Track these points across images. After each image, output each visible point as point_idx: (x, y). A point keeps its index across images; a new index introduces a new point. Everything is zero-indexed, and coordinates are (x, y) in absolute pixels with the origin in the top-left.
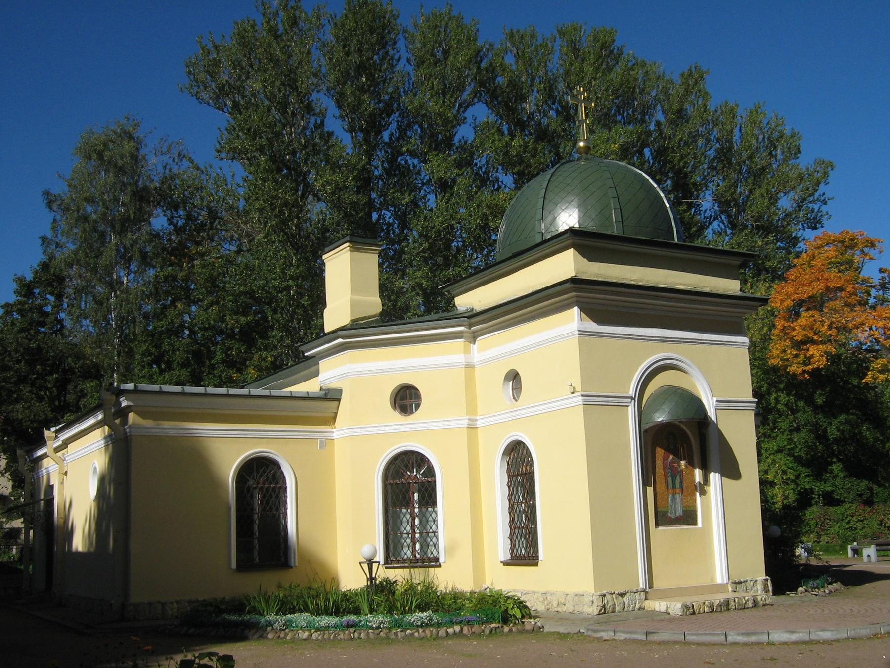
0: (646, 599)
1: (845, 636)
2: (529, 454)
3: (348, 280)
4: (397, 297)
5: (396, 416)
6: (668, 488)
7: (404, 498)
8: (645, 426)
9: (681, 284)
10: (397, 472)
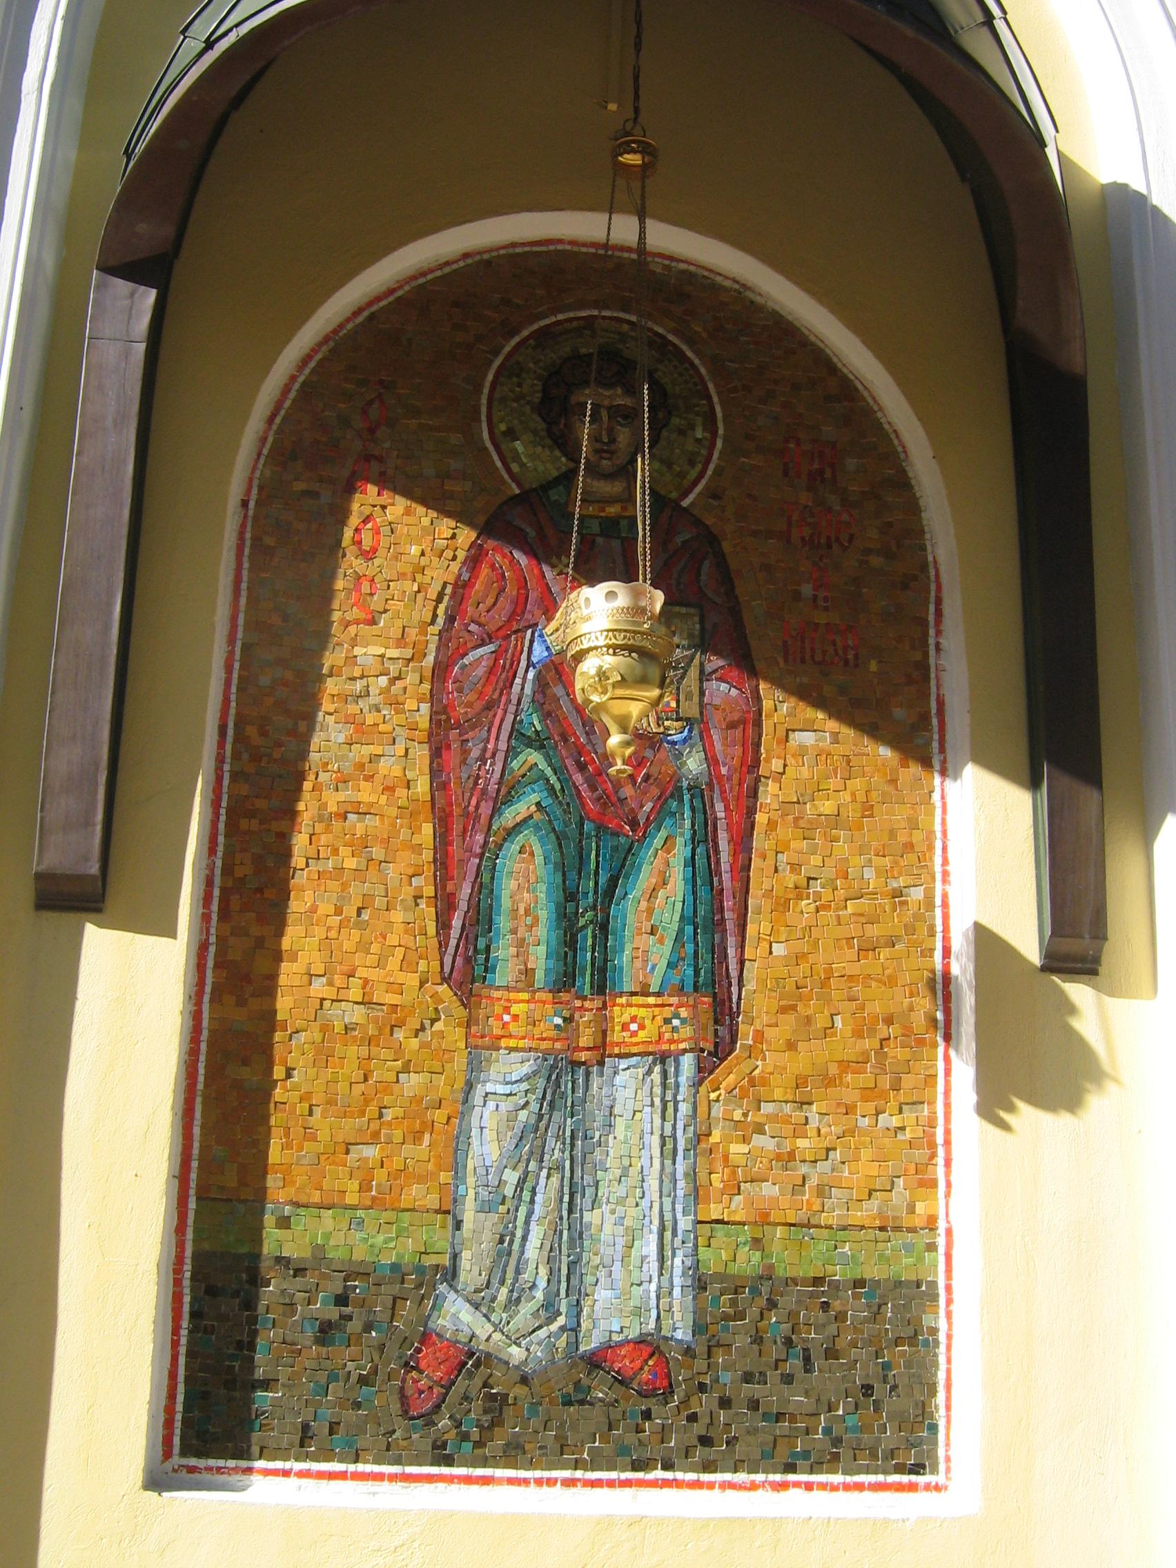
6: (468, 972)
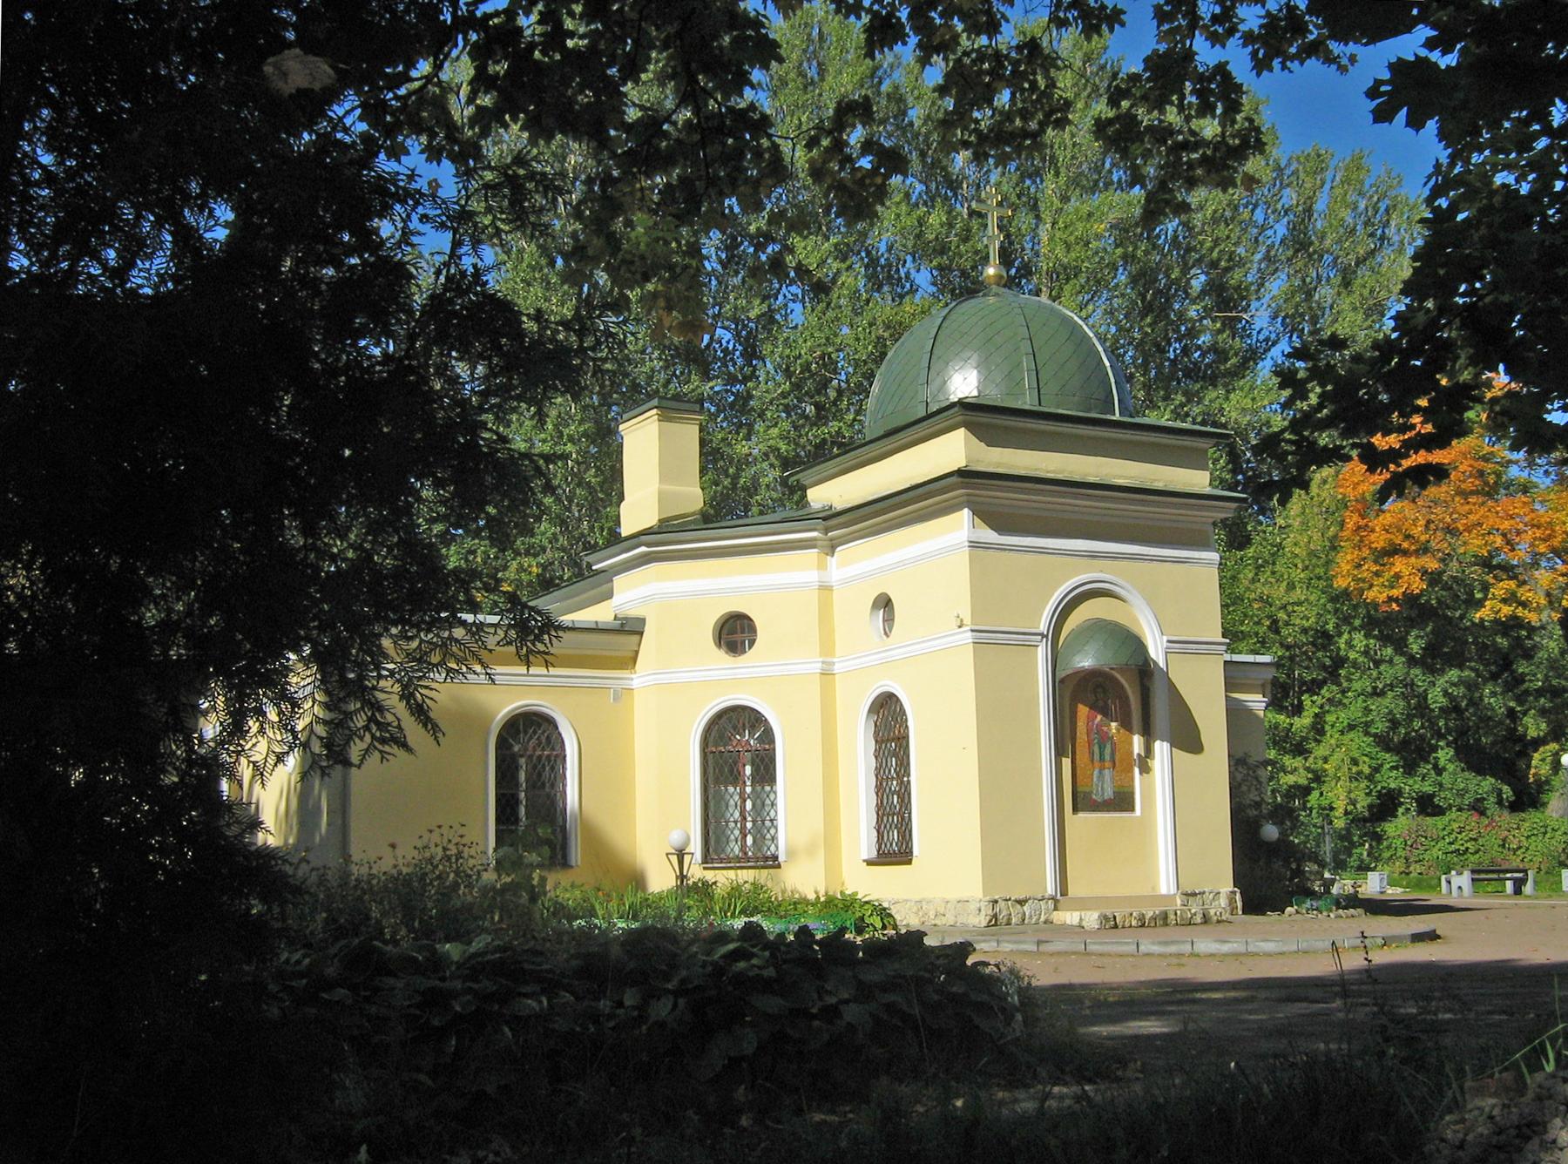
0: (1056, 909)
1: (1295, 948)
2: (904, 713)
3: (654, 463)
4: (739, 469)
5: (722, 657)
7: (731, 771)
8: (1061, 674)
9: (1120, 477)
10: (721, 737)
